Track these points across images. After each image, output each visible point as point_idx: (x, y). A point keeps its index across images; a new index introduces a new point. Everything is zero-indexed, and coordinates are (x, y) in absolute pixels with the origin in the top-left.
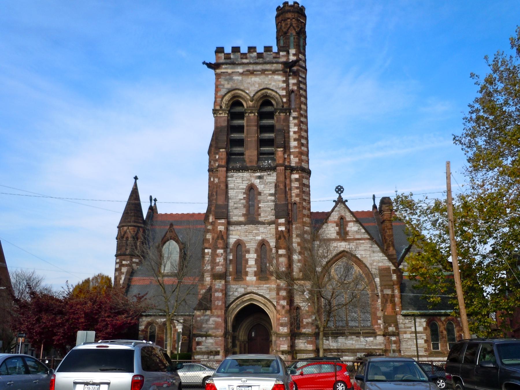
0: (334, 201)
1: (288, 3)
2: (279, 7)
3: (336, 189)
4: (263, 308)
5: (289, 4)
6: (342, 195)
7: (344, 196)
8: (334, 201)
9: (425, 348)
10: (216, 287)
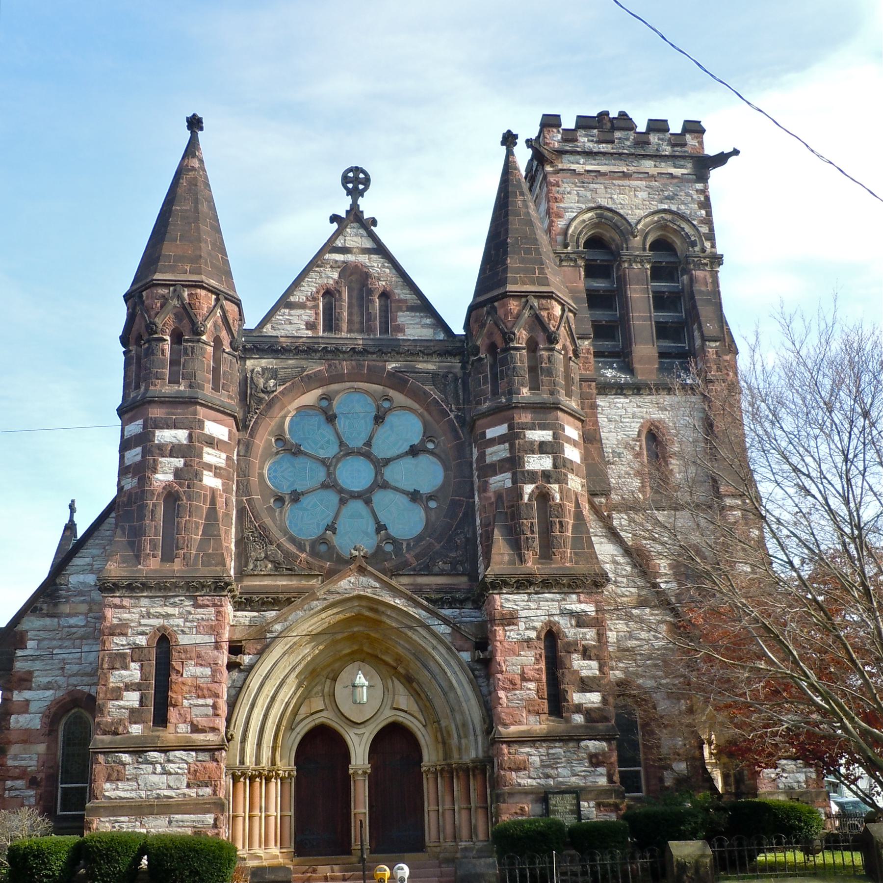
0: (334, 218)
1: (608, 114)
2: (607, 114)
3: (351, 170)
4: (294, 752)
5: (611, 116)
6: (361, 201)
7: (368, 206)
8: (334, 218)
9: (295, 856)
10: (497, 597)
